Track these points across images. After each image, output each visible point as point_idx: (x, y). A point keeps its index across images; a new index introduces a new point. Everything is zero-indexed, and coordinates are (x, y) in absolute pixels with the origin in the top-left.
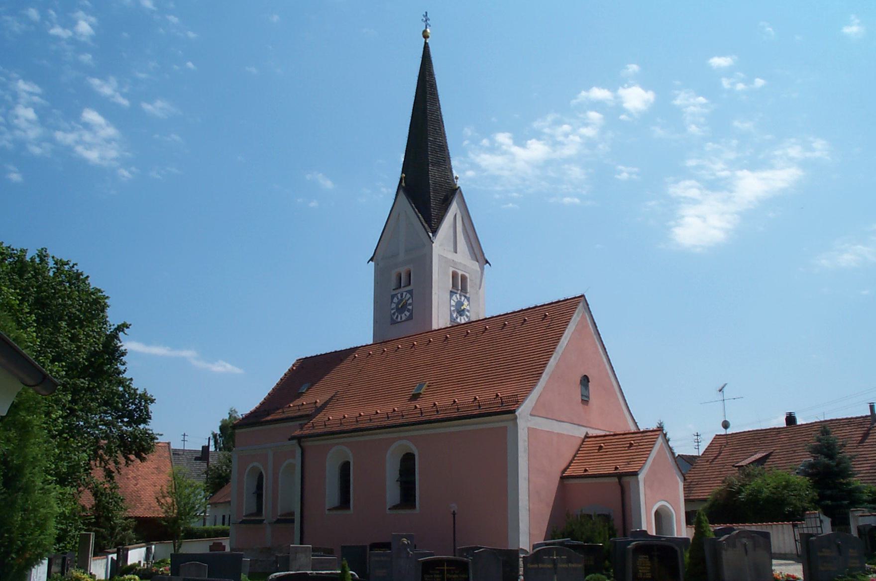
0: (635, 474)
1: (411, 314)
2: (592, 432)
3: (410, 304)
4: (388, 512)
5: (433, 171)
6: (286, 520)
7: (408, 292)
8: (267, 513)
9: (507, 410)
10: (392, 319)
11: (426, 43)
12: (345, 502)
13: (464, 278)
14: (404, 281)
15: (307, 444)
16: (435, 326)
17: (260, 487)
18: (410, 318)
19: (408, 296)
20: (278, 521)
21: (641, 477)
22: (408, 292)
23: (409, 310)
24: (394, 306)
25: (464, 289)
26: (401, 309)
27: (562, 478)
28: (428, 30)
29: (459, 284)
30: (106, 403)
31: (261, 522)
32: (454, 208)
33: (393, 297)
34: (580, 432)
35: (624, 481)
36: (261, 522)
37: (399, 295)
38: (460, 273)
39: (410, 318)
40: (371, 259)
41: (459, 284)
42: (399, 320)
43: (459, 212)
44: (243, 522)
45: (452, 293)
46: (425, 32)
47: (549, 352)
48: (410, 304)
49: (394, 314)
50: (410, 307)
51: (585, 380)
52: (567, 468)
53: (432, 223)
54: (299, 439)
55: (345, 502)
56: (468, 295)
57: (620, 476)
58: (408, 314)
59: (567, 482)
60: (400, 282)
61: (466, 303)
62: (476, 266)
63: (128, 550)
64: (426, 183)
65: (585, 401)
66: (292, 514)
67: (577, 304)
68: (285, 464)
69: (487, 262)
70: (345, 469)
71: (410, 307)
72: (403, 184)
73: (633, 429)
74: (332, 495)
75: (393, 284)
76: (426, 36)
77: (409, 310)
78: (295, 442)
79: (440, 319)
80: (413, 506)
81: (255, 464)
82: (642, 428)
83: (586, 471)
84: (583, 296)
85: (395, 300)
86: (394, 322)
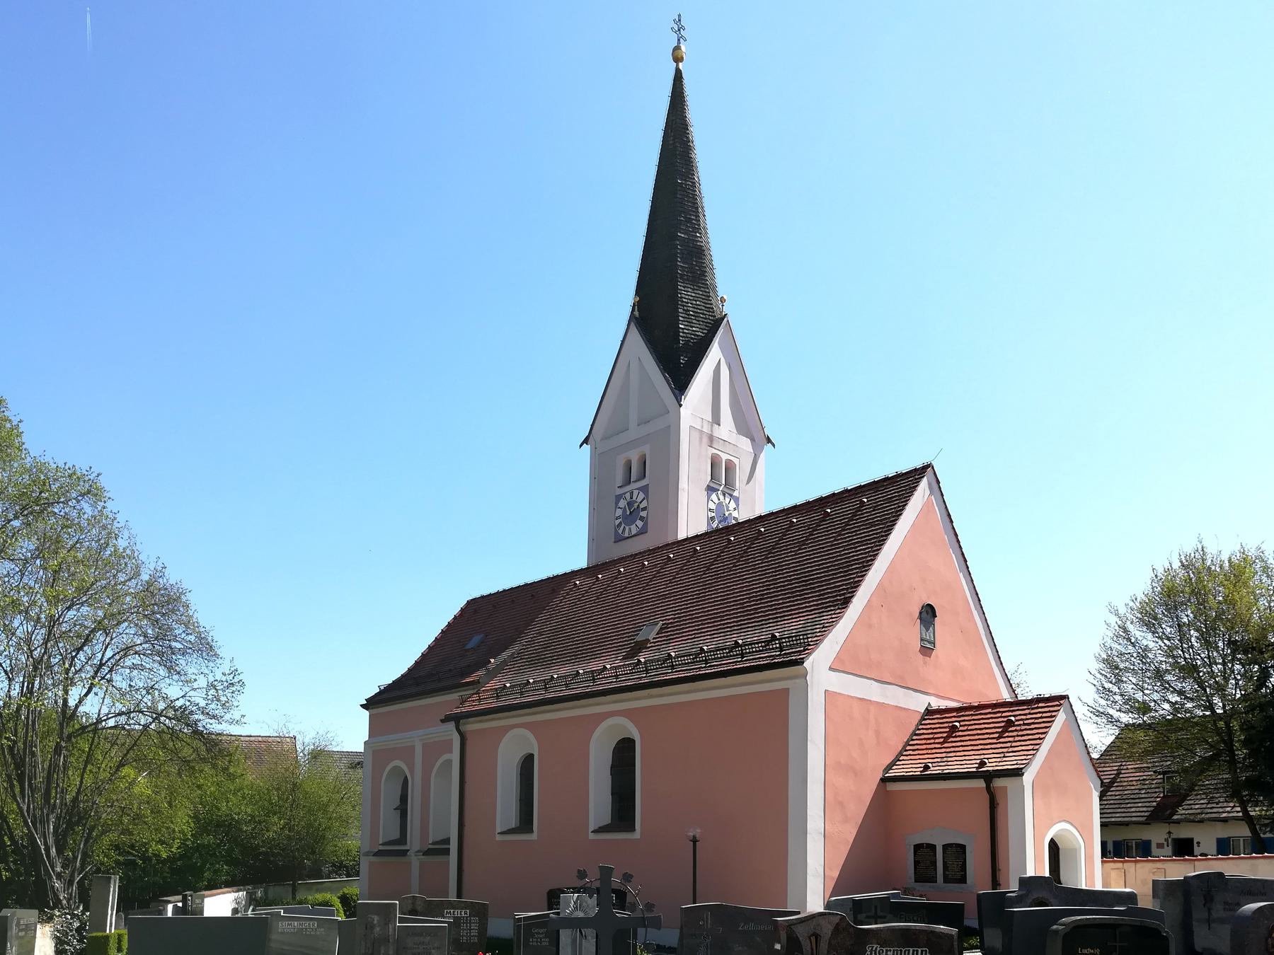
0: (1018, 773)
1: (646, 525)
2: (936, 703)
3: (644, 509)
4: (592, 836)
5: (686, 293)
6: (440, 849)
7: (642, 489)
8: (414, 842)
9: (791, 657)
10: (616, 532)
11: (678, 77)
12: (525, 822)
13: (730, 467)
14: (637, 472)
15: (471, 726)
16: (682, 535)
17: (404, 798)
18: (643, 531)
19: (642, 496)
20: (428, 852)
21: (1028, 777)
22: (642, 489)
23: (642, 519)
24: (619, 512)
25: (730, 484)
26: (632, 513)
27: (884, 780)
28: (683, 48)
29: (722, 478)
30: (161, 654)
31: (404, 853)
32: (714, 354)
33: (619, 498)
34: (919, 703)
35: (993, 787)
36: (404, 853)
37: (628, 496)
38: (724, 457)
39: (643, 531)
40: (586, 441)
41: (722, 478)
42: (626, 535)
43: (723, 360)
44: (379, 853)
45: (710, 489)
46: (677, 48)
47: (866, 566)
48: (644, 509)
49: (620, 525)
50: (643, 514)
51: (928, 613)
52: (893, 764)
53: (680, 379)
54: (457, 719)
55: (525, 822)
56: (736, 494)
57: (989, 777)
58: (640, 524)
59: (892, 787)
60: (629, 470)
61: (732, 505)
62: (745, 444)
63: (203, 897)
64: (674, 314)
65: (927, 649)
66: (447, 841)
67: (918, 481)
68: (438, 764)
69: (769, 440)
70: (528, 761)
71: (643, 514)
72: (636, 313)
73: (1006, 696)
74: (506, 811)
75: (619, 477)
76: (678, 59)
77: (642, 519)
78: (452, 725)
79: (692, 519)
80: (631, 828)
81: (534, 836)
82: (1025, 693)
83: (926, 768)
84: (929, 466)
85: (622, 503)
86: (619, 539)
